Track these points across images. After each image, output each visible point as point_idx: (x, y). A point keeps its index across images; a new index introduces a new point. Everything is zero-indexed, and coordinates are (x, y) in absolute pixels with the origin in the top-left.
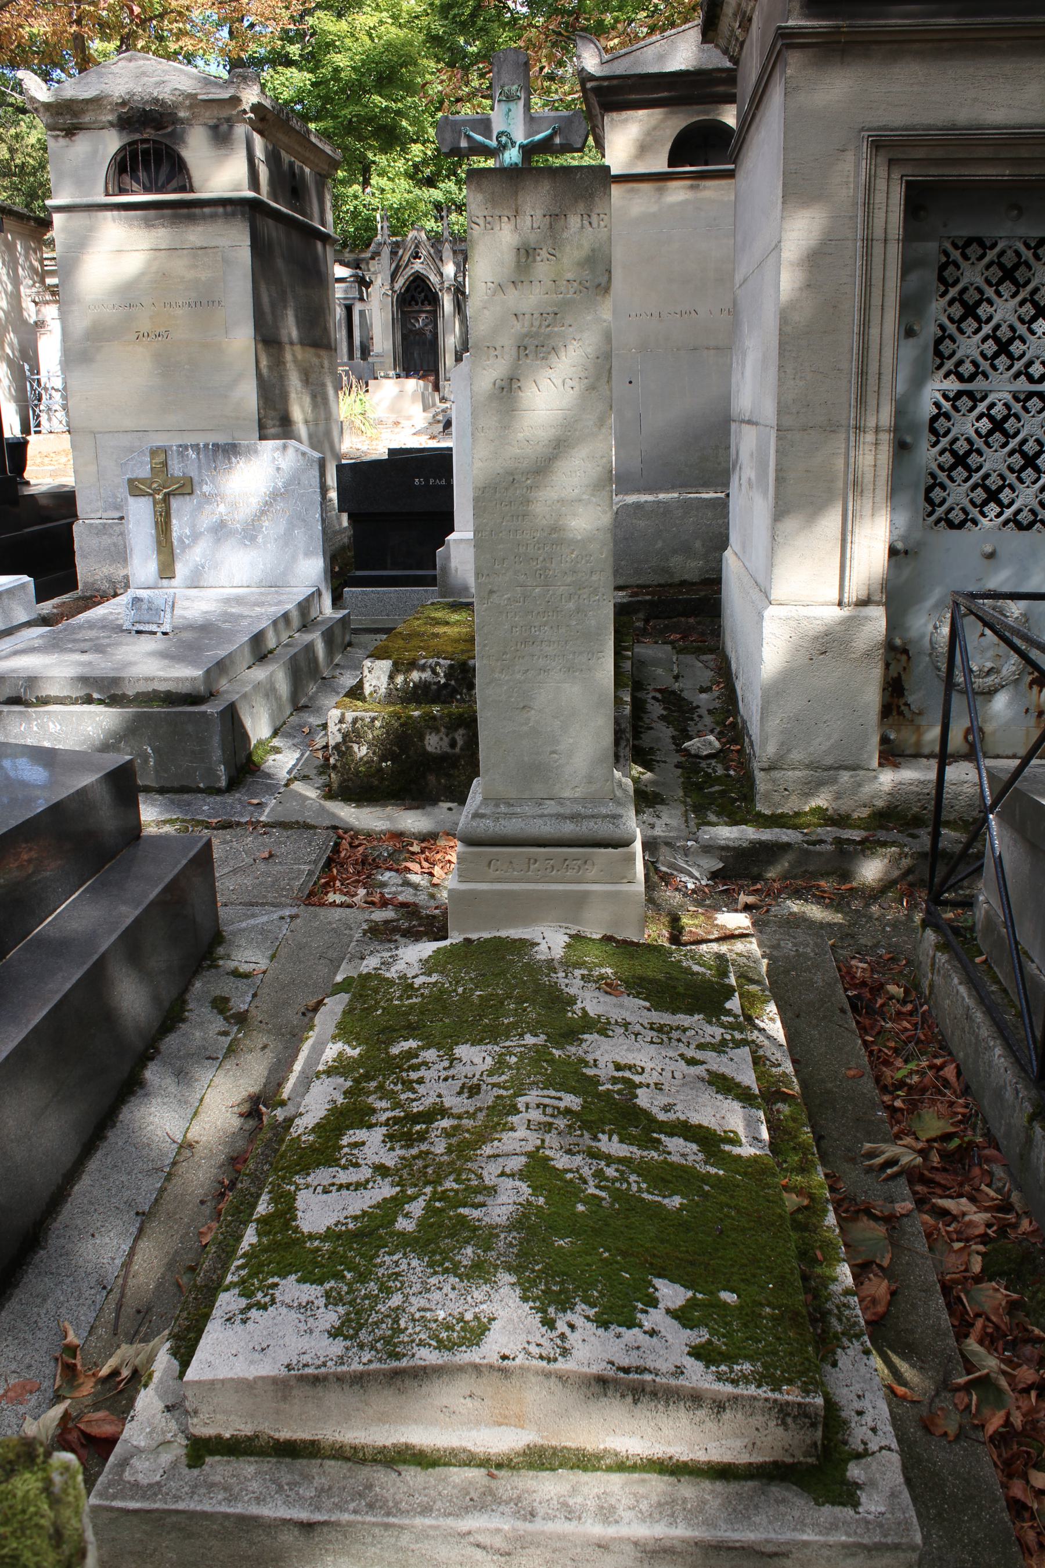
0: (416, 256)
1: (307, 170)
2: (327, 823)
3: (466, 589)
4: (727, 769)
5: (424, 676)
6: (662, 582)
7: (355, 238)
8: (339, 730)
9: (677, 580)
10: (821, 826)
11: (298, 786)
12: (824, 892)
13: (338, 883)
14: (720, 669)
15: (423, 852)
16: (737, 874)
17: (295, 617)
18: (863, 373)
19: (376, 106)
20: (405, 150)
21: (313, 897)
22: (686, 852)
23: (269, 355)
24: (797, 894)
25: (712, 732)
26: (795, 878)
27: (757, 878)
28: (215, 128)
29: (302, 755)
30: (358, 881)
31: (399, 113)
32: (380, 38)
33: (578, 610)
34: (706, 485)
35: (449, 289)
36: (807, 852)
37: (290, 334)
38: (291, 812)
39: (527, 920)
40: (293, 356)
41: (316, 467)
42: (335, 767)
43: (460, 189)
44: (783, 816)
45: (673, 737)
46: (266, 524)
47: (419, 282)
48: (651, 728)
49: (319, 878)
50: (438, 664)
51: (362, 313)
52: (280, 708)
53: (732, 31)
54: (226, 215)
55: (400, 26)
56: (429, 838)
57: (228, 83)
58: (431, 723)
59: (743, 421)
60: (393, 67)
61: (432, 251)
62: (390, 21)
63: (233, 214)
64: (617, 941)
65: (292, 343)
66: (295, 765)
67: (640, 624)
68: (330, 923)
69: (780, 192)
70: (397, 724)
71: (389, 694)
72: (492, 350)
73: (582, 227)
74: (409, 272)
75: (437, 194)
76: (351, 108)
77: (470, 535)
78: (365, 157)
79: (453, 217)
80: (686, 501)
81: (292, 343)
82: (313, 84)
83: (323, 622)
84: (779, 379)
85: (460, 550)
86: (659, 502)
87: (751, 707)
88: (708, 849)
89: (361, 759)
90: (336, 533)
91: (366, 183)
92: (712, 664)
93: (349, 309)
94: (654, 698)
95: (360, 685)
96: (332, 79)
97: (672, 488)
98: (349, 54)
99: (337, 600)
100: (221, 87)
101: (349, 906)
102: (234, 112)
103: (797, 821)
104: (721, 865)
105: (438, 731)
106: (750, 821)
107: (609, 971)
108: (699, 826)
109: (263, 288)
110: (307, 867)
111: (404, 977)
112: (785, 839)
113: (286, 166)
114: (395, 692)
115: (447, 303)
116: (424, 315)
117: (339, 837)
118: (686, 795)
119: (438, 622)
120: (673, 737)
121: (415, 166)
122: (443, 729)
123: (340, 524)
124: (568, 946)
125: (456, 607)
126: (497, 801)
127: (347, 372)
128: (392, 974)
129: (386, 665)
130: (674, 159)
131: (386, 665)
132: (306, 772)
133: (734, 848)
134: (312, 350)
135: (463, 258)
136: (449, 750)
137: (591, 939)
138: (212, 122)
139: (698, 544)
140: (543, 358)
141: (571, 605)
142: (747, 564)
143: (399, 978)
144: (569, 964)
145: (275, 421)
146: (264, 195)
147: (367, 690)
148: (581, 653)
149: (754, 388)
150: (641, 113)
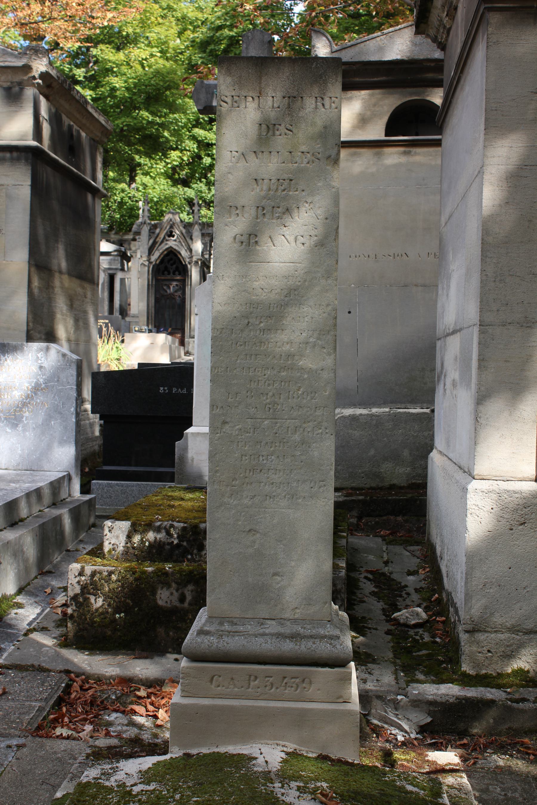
0: (171, 235)
1: (83, 134)
2: (61, 667)
3: (200, 477)
4: (434, 636)
5: (159, 536)
6: (374, 485)
7: (121, 223)
8: (78, 582)
9: (387, 484)
10: (523, 686)
11: (36, 636)
12: (529, 748)
13: (66, 719)
14: (426, 557)
15: (149, 697)
16: (444, 725)
17: (47, 492)
19: (143, 119)
20: (165, 155)
21: (42, 730)
22: (396, 705)
23: (40, 278)
24: (502, 749)
25: (419, 606)
26: (500, 734)
27: (463, 734)
28: (8, 90)
29: (43, 611)
30: (85, 720)
31: (162, 125)
32: (150, 67)
33: (303, 442)
34: (414, 401)
35: (196, 262)
36: (510, 708)
37: (59, 265)
38: (28, 657)
39: (247, 737)
40: (62, 283)
41: (74, 367)
42: (72, 617)
43: (209, 189)
44: (486, 676)
45: (383, 610)
46: (27, 414)
47: (172, 256)
48: (364, 602)
49: (48, 714)
50: (172, 526)
51: (122, 281)
52: (27, 570)
53: (441, 21)
54: (12, 159)
55: (167, 59)
56: (155, 685)
57: (24, 52)
58: (163, 579)
60: (159, 90)
61: (184, 231)
62: (159, 54)
63: (18, 159)
64: (332, 760)
65: (61, 272)
66: (35, 619)
67: (354, 520)
68: (55, 753)
69: (482, 127)
70: (131, 579)
71: (126, 552)
72: (233, 209)
73: (316, 108)
74: (164, 247)
75: (190, 193)
76: (123, 119)
77: (206, 430)
78: (133, 159)
79: (204, 211)
80: (396, 415)
81: (61, 272)
82: (93, 99)
83: (71, 502)
84: (482, 282)
85: (197, 442)
86: (372, 415)
87: (455, 578)
88: (417, 703)
89: (97, 610)
90: (88, 440)
91: (132, 180)
92: (418, 553)
93: (112, 278)
94: (366, 578)
95: (101, 546)
96: (108, 96)
97: (384, 403)
98: (124, 78)
99: (85, 489)
100: (16, 57)
101: (74, 739)
102: (25, 78)
103: (500, 681)
104: (429, 720)
105: (169, 586)
106: (456, 680)
107: (325, 785)
108: (408, 683)
109: (39, 221)
110: (38, 704)
111: (123, 785)
112: (489, 696)
113: (65, 128)
114: (131, 551)
115: (195, 274)
116: (175, 283)
117: (71, 680)
118: (395, 657)
119: (173, 498)
120: (383, 610)
121: (174, 169)
122: (174, 585)
123: (93, 433)
124: (284, 761)
125: (191, 489)
126: (222, 620)
127: (107, 325)
128: (112, 782)
129: (125, 525)
130: (390, 130)
131: (125, 525)
132: (45, 624)
133: (442, 703)
134: (78, 282)
135: (209, 238)
136: (178, 604)
137: (306, 757)
138: (6, 85)
139: (406, 453)
140: (278, 218)
141: (297, 437)
142: (451, 455)
143: (118, 786)
144: (285, 776)
145: (40, 329)
146: (46, 146)
147: (107, 547)
148: (304, 481)
149: (458, 302)
150: (363, 92)
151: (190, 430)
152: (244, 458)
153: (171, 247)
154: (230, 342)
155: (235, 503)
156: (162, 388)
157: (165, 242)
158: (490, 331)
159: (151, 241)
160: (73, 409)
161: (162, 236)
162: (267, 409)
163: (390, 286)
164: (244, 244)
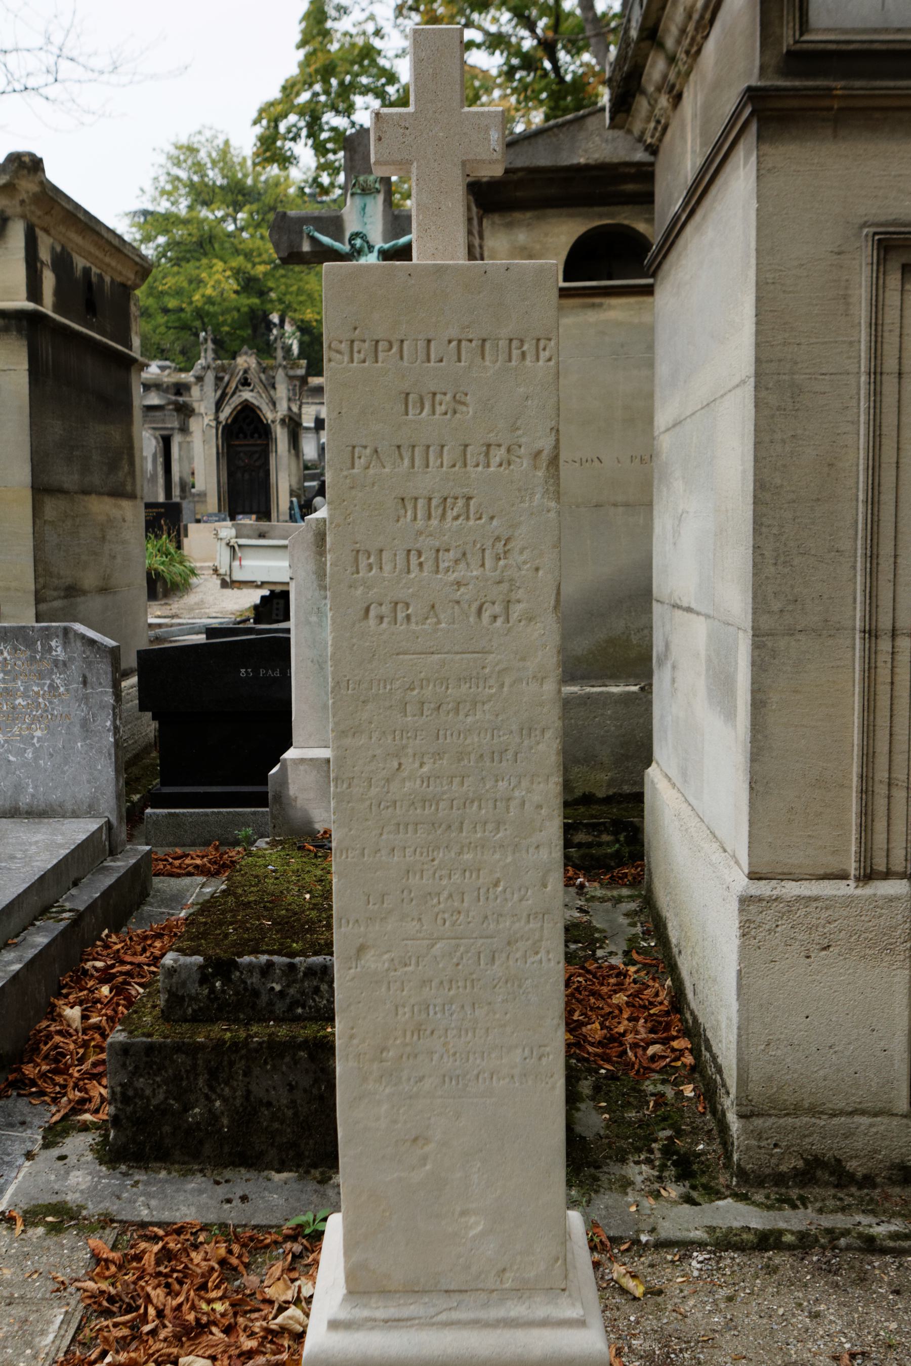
18: (872, 557)
34: (615, 676)
47: (247, 412)
59: (676, 606)
74: (236, 401)
84: (755, 565)
115: (281, 435)
146: (47, 308)
151: (290, 754)
152: (400, 1012)
153: (246, 400)
154: (368, 803)
155: (387, 1091)
156: (243, 671)
157: (238, 394)
158: (770, 644)
159: (219, 393)
160: (108, 723)
161: (233, 385)
162: (440, 921)
163: (577, 507)
164: (386, 620)
